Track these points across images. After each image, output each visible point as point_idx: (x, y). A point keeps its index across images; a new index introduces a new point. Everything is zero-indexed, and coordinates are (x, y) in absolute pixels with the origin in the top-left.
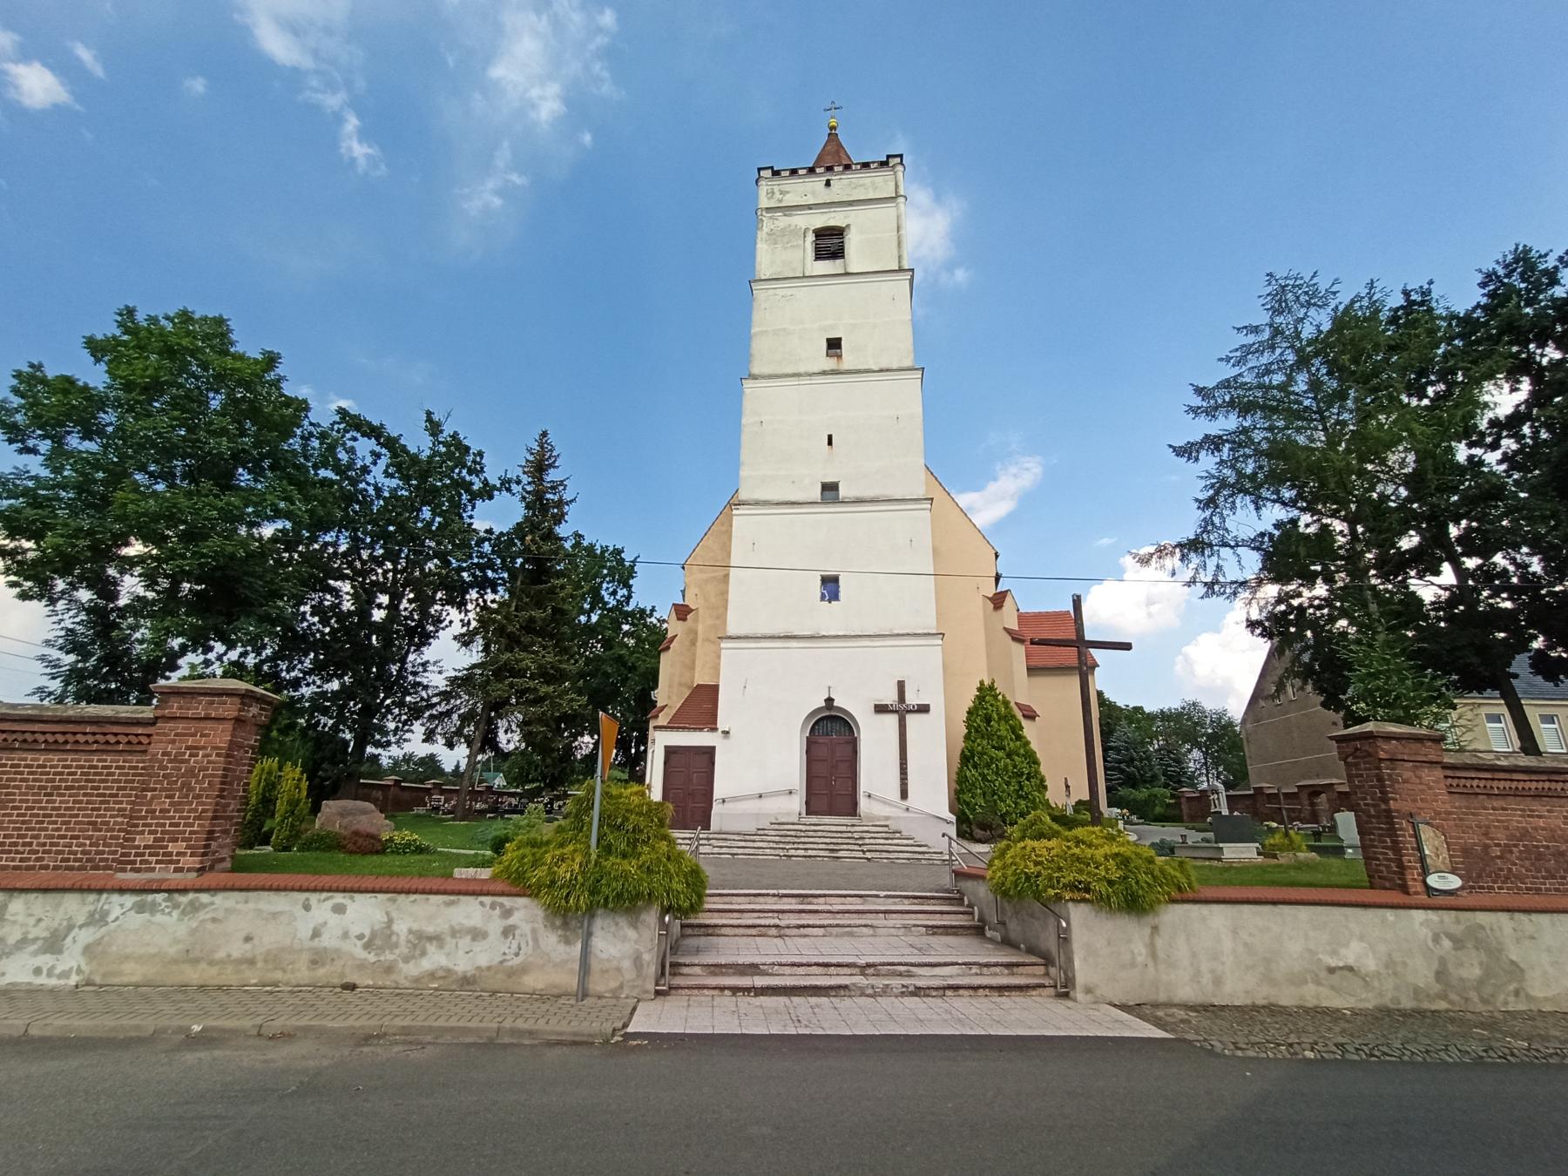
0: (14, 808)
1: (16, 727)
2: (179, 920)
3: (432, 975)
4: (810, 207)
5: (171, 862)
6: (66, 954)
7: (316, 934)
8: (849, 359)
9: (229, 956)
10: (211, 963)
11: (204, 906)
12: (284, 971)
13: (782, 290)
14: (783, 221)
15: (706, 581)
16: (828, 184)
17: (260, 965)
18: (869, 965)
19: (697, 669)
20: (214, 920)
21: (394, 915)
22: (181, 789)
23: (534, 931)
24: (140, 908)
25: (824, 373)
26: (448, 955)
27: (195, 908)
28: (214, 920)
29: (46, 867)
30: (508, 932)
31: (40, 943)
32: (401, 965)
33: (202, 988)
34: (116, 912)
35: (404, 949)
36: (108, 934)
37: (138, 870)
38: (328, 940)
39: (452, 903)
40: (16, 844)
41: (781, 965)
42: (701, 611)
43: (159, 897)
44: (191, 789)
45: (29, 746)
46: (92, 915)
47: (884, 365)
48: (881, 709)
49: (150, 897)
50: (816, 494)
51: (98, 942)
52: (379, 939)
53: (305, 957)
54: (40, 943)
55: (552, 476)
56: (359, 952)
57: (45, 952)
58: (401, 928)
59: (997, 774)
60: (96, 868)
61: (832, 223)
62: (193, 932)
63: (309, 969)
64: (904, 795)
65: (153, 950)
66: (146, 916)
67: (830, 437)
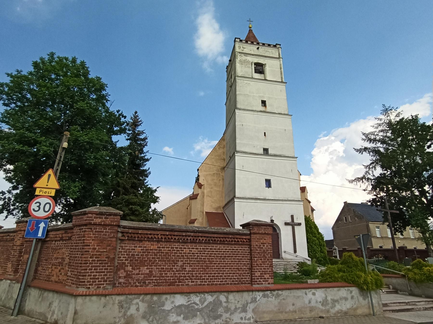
0: (214, 264)
1: (210, 235)
2: (275, 300)
3: (338, 312)
4: (253, 55)
5: (266, 281)
6: (248, 312)
7: (310, 302)
8: (269, 109)
9: (290, 310)
10: (286, 313)
11: (280, 295)
12: (304, 314)
13: (246, 81)
14: (244, 58)
15: (207, 175)
16: (258, 48)
17: (297, 312)
18: (408, 302)
19: (205, 206)
20: (284, 299)
21: (327, 295)
22: (263, 257)
23: (357, 297)
24: (264, 296)
25: (261, 111)
26: (340, 306)
27: (278, 296)
28: (284, 299)
29: (228, 284)
30: (352, 297)
31: (240, 309)
32: (331, 310)
33: (286, 320)
34: (258, 298)
35: (330, 305)
36: (258, 305)
37: (258, 284)
38: (313, 304)
39: (338, 290)
40: (218, 276)
41: (391, 303)
42: (205, 185)
43: (268, 292)
44: (266, 257)
45: (215, 242)
46: (252, 299)
47: (280, 112)
48: (286, 224)
49: (266, 293)
50: (261, 151)
51: (256, 308)
52: (324, 302)
53: (308, 310)
54: (240, 309)
55: (140, 129)
56: (321, 307)
57: (242, 312)
58: (329, 298)
59: (315, 245)
60: (242, 284)
61: (260, 62)
62: (279, 303)
63: (310, 313)
64: (295, 251)
65: (271, 310)
66: (266, 298)
67: (265, 133)
